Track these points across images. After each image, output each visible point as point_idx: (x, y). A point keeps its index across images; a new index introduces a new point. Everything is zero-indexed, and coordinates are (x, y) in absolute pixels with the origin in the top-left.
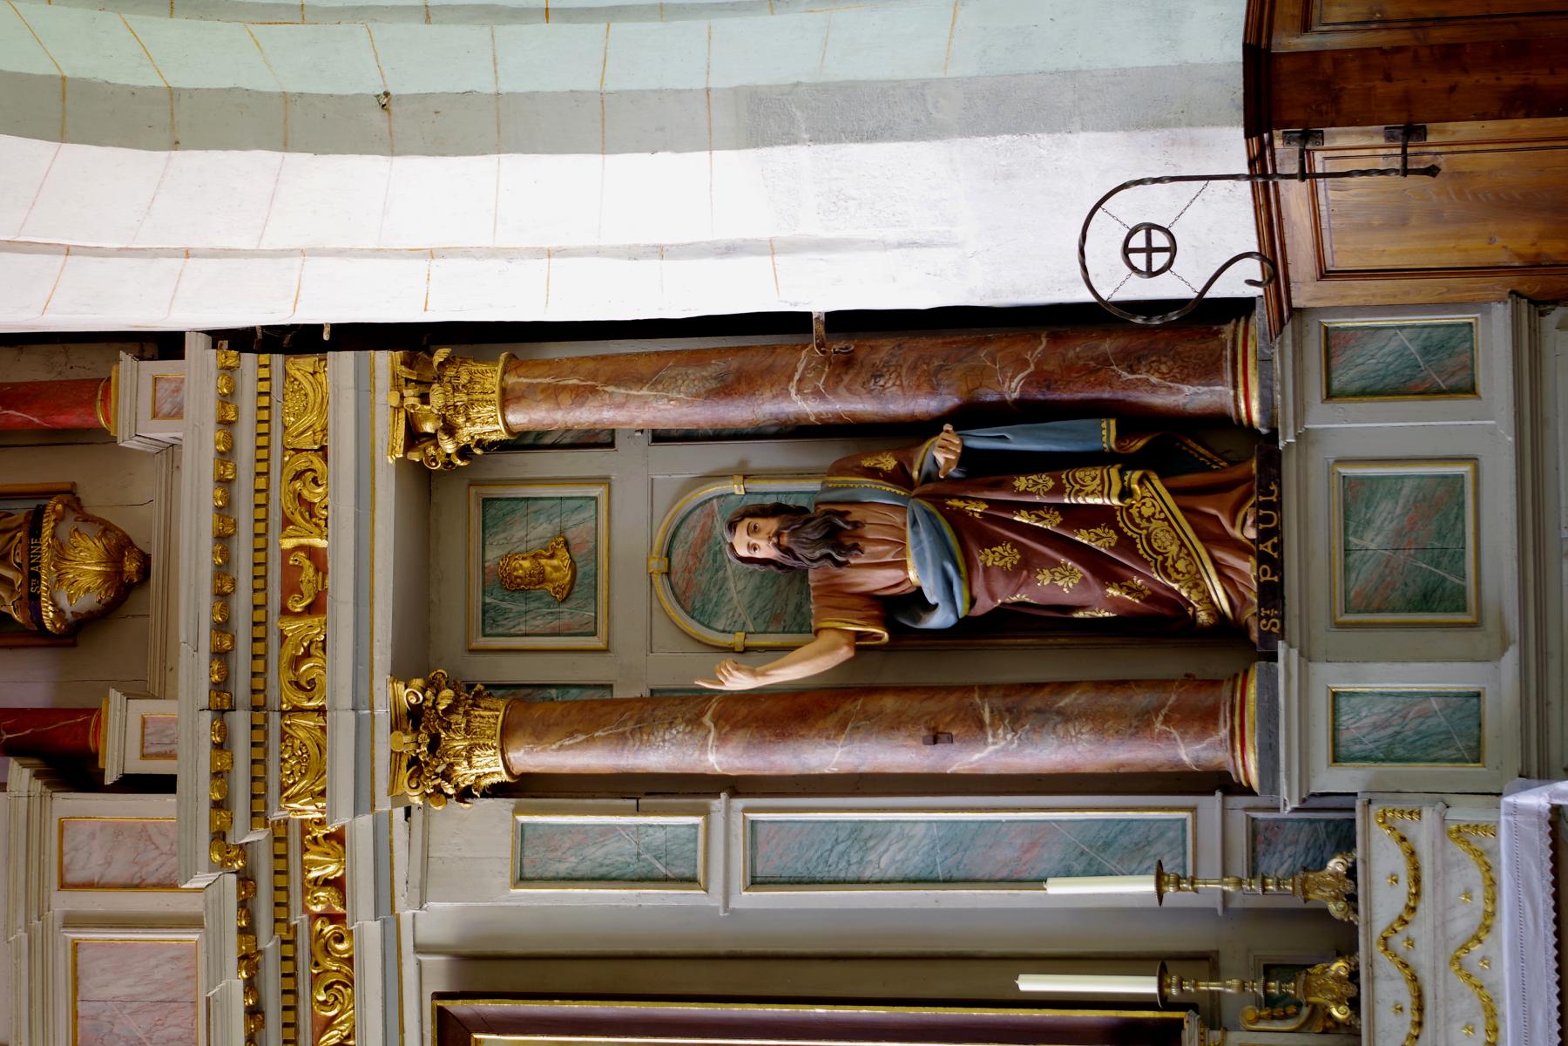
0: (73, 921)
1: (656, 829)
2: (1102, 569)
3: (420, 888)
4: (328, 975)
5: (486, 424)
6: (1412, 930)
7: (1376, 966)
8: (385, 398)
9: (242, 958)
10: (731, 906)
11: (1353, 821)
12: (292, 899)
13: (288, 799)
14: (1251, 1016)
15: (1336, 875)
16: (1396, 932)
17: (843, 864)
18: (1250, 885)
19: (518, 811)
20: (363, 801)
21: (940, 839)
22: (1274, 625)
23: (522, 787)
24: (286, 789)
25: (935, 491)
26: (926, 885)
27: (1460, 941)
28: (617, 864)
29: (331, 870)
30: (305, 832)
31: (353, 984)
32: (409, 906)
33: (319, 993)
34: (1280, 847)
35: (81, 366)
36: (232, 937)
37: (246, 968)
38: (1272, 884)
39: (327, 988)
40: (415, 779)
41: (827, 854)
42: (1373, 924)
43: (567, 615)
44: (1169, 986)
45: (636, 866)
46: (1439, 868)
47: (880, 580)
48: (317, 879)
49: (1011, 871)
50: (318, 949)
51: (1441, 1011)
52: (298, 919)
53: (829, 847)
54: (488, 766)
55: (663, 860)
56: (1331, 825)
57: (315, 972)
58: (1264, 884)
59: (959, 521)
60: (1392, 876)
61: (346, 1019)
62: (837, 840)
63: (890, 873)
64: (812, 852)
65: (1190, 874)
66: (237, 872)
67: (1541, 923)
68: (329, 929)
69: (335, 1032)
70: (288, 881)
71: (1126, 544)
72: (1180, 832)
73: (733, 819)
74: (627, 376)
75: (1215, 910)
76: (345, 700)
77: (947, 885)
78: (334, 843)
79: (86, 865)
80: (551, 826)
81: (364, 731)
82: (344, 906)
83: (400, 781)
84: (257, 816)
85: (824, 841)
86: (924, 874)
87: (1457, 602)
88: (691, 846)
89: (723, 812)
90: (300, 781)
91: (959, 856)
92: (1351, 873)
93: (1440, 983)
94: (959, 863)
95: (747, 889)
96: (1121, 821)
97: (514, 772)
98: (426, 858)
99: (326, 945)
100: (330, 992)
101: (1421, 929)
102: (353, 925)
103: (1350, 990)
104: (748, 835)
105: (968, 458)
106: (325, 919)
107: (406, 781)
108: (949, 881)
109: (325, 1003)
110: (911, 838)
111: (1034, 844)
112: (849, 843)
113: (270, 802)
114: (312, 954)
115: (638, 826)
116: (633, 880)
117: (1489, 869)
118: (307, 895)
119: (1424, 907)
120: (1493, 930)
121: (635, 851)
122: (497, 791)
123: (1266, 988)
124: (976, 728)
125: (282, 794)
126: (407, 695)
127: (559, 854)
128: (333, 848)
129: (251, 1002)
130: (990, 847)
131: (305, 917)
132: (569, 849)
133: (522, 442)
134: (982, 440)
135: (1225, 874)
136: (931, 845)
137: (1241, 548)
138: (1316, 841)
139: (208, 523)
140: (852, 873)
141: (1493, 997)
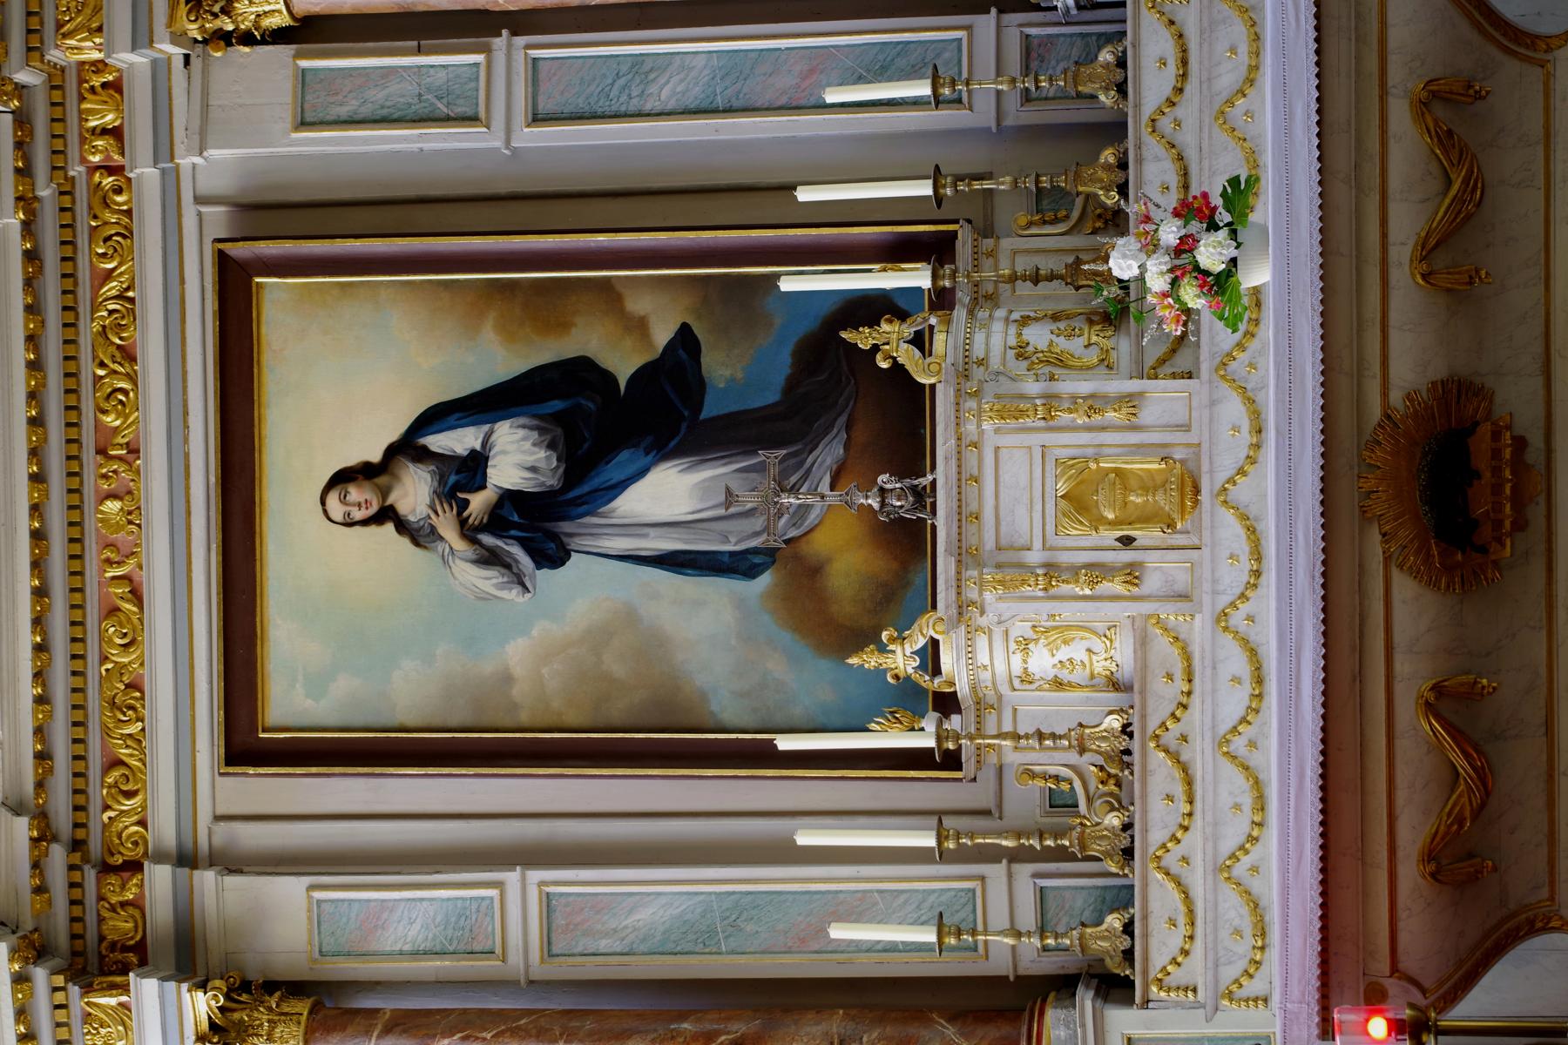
1: (438, 69)
3: (200, 134)
4: (107, 227)
6: (1179, 112)
7: (1144, 148)
9: (18, 199)
10: (514, 144)
11: (1132, 887)
12: (69, 148)
13: (65, 36)
14: (1023, 221)
15: (1106, 66)
16: (1164, 114)
17: (624, 98)
18: (1024, 82)
19: (299, 55)
21: (720, 69)
24: (63, 26)
26: (705, 115)
27: (1225, 96)
28: (398, 105)
29: (110, 119)
30: (81, 81)
31: (132, 234)
32: (189, 152)
33: (98, 246)
34: (1053, 63)
36: (20, 371)
37: (23, 208)
38: (1045, 81)
39: (107, 240)
40: (194, 14)
41: (608, 88)
42: (1142, 108)
44: (944, 186)
45: (417, 107)
46: (1206, 24)
48: (94, 128)
49: (790, 99)
50: (96, 202)
51: (1206, 163)
52: (76, 170)
53: (610, 81)
55: (445, 101)
56: (1103, 38)
57: (94, 224)
58: (1037, 81)
60: (1161, 59)
61: (125, 270)
62: (617, 74)
63: (670, 106)
64: (592, 87)
65: (965, 75)
66: (12, 112)
67: (1303, 18)
68: (108, 181)
69: (115, 284)
70: (65, 129)
72: (956, 51)
73: (515, 57)
75: (990, 128)
77: (726, 115)
78: (112, 92)
80: (332, 70)
82: (122, 154)
83: (179, 15)
85: (604, 76)
86: (704, 105)
88: (473, 85)
89: (504, 48)
90: (77, 16)
91: (739, 85)
92: (1122, 63)
93: (1206, 135)
94: (739, 92)
95: (528, 126)
96: (898, 43)
97: (294, 12)
98: (205, 107)
99: (104, 198)
100: (109, 243)
101: (1188, 109)
102: (131, 171)
103: (1119, 177)
104: (530, 73)
106: (103, 171)
107: (185, 18)
108: (729, 111)
109: (104, 255)
110: (691, 69)
111: (812, 71)
112: (630, 76)
113: (46, 38)
114: (90, 208)
115: (420, 67)
116: (414, 121)
117: (1254, 24)
118: (85, 144)
119: (1191, 87)
120: (1257, 84)
121: (417, 92)
123: (1037, 182)
125: (57, 31)
127: (340, 97)
128: (112, 97)
129: (28, 246)
130: (770, 75)
131: (81, 169)
132: (350, 92)
135: (999, 73)
136: (711, 76)
138: (1087, 55)
140: (634, 106)
141: (1256, 149)
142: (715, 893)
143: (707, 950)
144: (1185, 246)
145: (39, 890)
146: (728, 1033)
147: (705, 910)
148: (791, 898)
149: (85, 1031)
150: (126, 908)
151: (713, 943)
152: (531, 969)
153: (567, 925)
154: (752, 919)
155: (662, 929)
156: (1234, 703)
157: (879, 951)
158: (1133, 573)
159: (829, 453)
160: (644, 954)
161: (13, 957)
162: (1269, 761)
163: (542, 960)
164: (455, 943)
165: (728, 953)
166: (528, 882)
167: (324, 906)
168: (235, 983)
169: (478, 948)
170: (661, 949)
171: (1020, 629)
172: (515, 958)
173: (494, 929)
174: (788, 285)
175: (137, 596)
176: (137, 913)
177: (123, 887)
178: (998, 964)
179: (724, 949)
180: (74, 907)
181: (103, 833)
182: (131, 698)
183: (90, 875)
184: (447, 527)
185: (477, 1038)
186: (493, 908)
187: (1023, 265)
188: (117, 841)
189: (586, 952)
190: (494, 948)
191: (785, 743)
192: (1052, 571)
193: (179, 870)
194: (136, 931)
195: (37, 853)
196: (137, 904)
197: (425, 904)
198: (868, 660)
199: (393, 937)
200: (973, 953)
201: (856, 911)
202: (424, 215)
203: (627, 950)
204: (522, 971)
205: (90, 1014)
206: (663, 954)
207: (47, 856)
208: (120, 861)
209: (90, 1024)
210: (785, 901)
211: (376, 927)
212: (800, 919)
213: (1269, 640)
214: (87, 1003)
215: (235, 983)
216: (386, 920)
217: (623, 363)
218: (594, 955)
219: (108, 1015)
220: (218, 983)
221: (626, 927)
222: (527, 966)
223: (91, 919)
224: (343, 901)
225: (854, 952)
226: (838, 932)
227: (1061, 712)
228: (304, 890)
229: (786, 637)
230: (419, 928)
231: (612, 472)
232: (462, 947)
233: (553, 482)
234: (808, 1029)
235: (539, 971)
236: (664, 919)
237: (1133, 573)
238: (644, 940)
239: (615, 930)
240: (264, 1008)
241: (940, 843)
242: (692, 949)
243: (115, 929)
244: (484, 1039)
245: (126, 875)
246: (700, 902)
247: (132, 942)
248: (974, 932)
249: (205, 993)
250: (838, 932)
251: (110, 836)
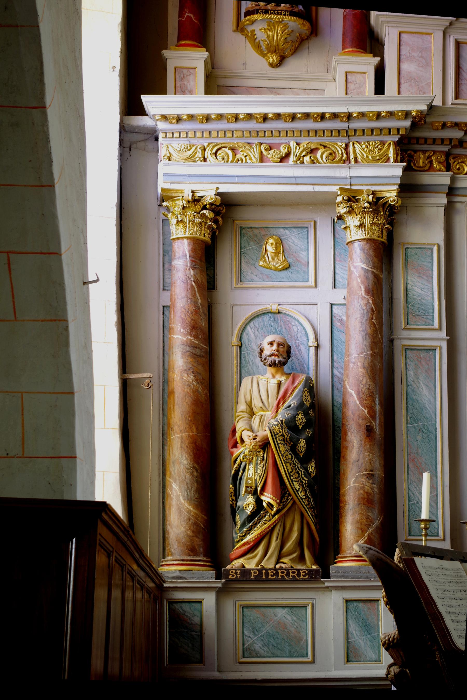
22: (233, 576)
36: (320, 110)
142: (436, 423)
143: (408, 418)
145: (444, 125)
146: (376, 425)
147: (428, 418)
148: (434, 456)
149: (377, 142)
150: (429, 163)
151: (412, 421)
152: (399, 341)
153: (420, 357)
154: (424, 439)
155: (419, 399)
157: (408, 493)
160: (407, 391)
161: (419, 112)
163: (403, 346)
164: (412, 308)
165: (407, 427)
166: (441, 341)
167: (430, 250)
168: (395, 209)
169: (410, 317)
170: (409, 398)
172: (405, 334)
173: (418, 325)
176: (427, 168)
177: (440, 162)
179: (409, 426)
180: (432, 140)
181: (464, 155)
182: (322, 159)
183: (445, 148)
185: (372, 315)
186: (429, 325)
188: (460, 161)
189: (407, 365)
190: (409, 325)
193: (447, 187)
194: (418, 167)
195: (462, 125)
196: (431, 168)
197: (431, 295)
199: (415, 280)
200: (408, 534)
203: (408, 383)
204: (399, 337)
205: (384, 144)
206: (407, 399)
207: (459, 130)
208: (451, 162)
209: (380, 144)
210: (432, 453)
211: (420, 273)
212: (424, 460)
214: (390, 144)
215: (395, 209)
216: (423, 278)
218: (406, 369)
219: (384, 152)
220: (400, 202)
221: (419, 383)
222: (401, 339)
223: (425, 147)
224: (432, 259)
225: (408, 482)
228: (437, 243)
230: (419, 292)
232: (410, 311)
234: (378, 461)
235: (398, 345)
236: (423, 400)
238: (413, 391)
239: (418, 378)
240: (385, 222)
242: (409, 411)
243: (420, 158)
244: (372, 319)
245: (445, 164)
246: (431, 416)
247: (412, 165)
248: (426, 535)
249: (396, 196)
250: (426, 476)
251: (462, 158)
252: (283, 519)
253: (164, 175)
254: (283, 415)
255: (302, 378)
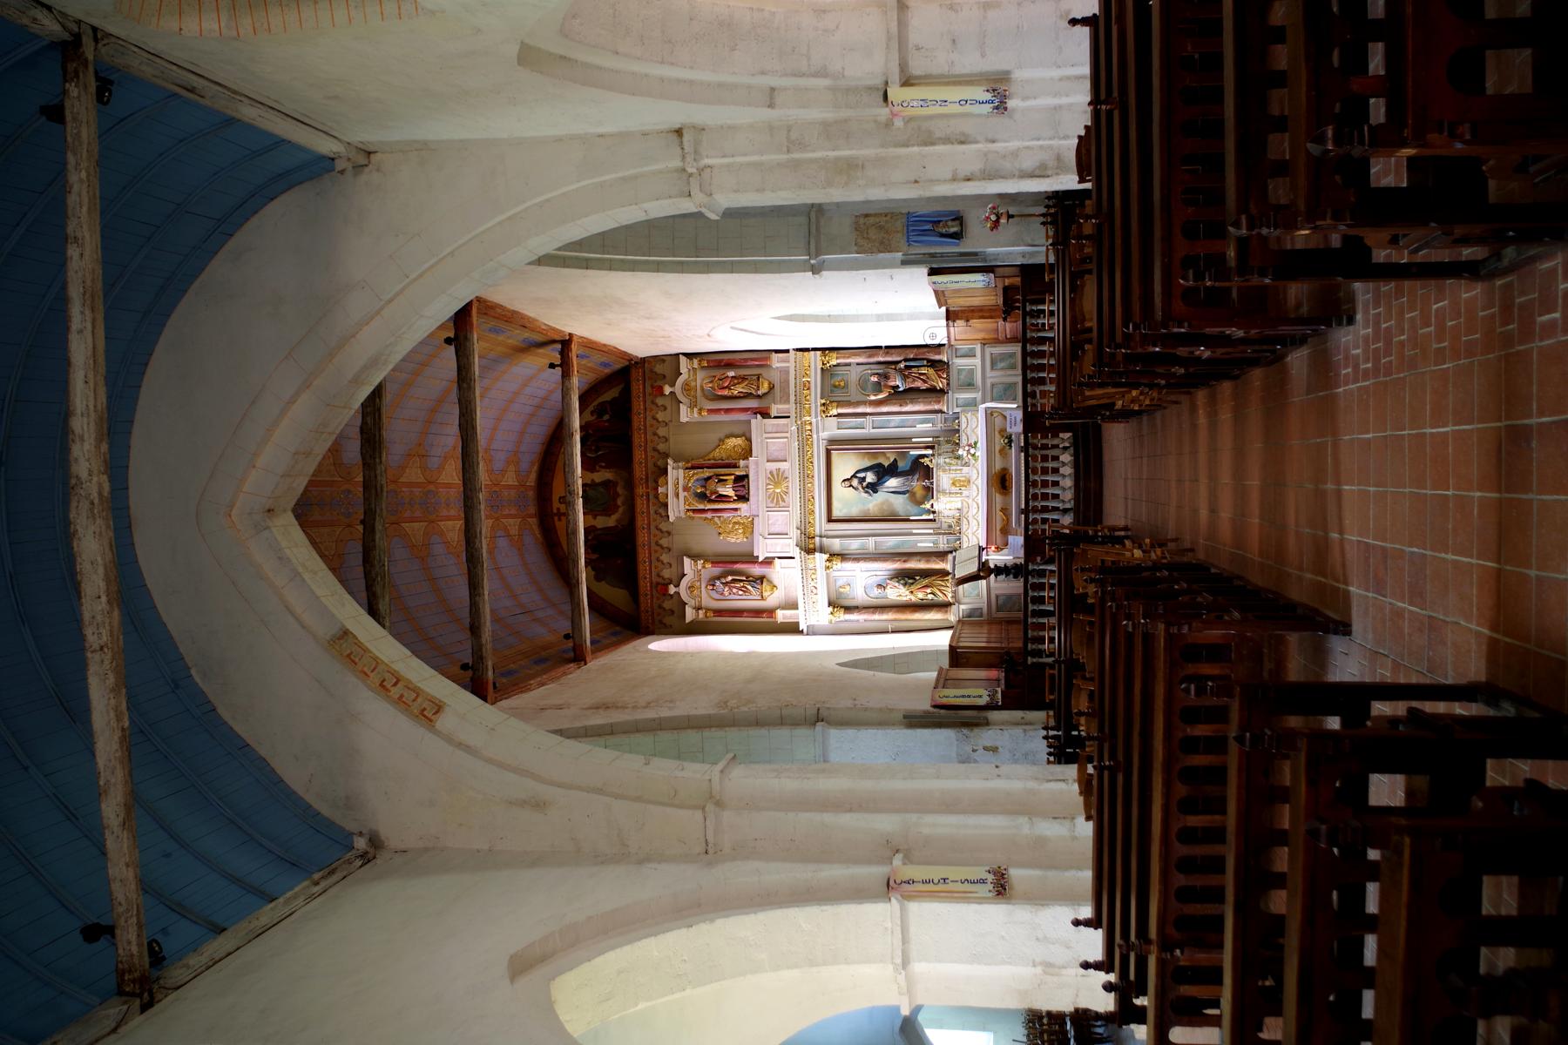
0: (766, 438)
2: (924, 381)
5: (834, 362)
8: (819, 358)
20: (816, 417)
23: (839, 415)
25: (901, 371)
29: (809, 428)
35: (764, 355)
43: (844, 391)
47: (892, 384)
54: (834, 412)
59: (904, 375)
71: (928, 378)
74: (855, 355)
76: (813, 401)
79: (770, 429)
81: (816, 407)
84: (801, 419)
87: (973, 385)
101: (968, 429)
105: (905, 366)
122: (834, 416)
124: (907, 404)
126: (823, 401)
133: (838, 365)
134: (907, 364)
137: (944, 378)
139: (794, 377)
144: (969, 450)
156: (975, 511)
158: (961, 493)
159: (916, 477)
162: (980, 519)
171: (945, 501)
174: (911, 453)
175: (813, 498)
178: (941, 550)
184: (860, 489)
187: (945, 450)
191: (911, 518)
192: (950, 493)
196: (814, 543)
198: (923, 506)
201: (921, 542)
202: (856, 442)
213: (980, 502)
217: (886, 464)
226: (919, 545)
227: (951, 513)
229: (911, 504)
231: (884, 480)
233: (876, 481)
237: (961, 493)
241: (1048, 538)
250: (919, 545)
252: (935, 586)
253: (830, 605)
254: (901, 587)
255: (888, 581)
